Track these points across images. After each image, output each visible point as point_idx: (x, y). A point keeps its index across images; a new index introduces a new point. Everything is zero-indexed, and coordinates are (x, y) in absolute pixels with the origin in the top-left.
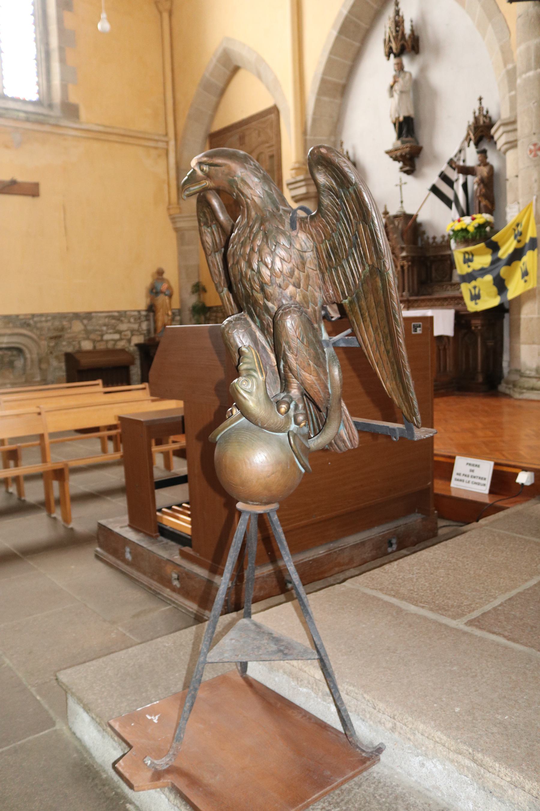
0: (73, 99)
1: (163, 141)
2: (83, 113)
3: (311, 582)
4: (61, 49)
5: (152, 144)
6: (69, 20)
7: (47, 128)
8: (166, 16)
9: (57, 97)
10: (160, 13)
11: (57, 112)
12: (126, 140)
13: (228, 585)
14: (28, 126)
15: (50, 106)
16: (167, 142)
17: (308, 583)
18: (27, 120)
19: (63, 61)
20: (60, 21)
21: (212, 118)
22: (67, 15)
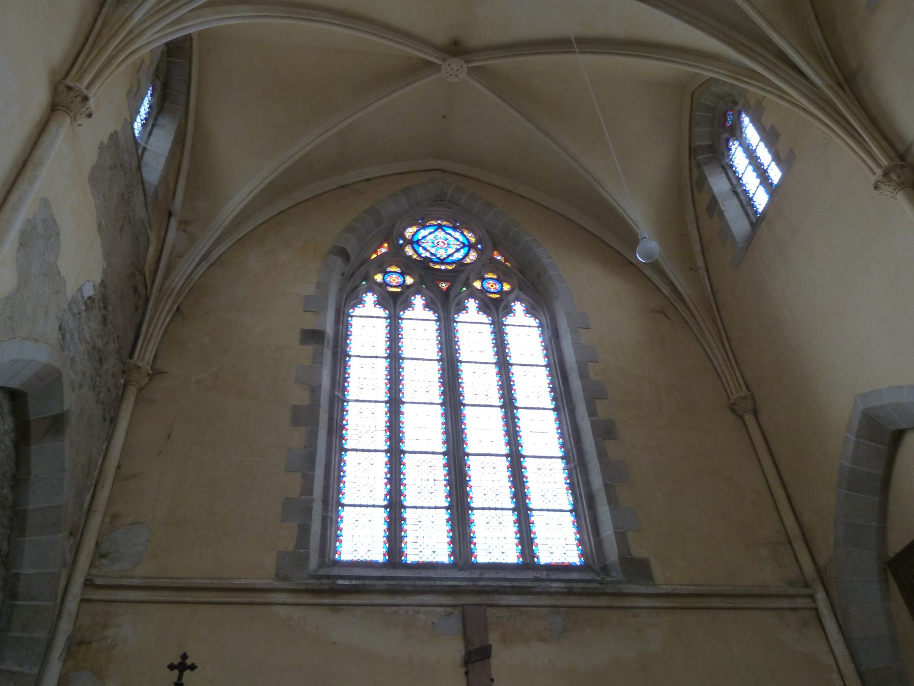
0: (638, 551)
1: (802, 596)
2: (657, 570)
3: (110, 496)
4: (608, 487)
5: (786, 603)
6: (612, 447)
7: (603, 601)
8: (749, 418)
9: (612, 553)
10: (741, 417)
11: (617, 575)
12: (739, 602)
13: (103, 267)
14: (573, 601)
15: (605, 569)
16: (812, 597)
17: (112, 489)
18: (570, 593)
19: (612, 501)
20: (602, 454)
21: (882, 532)
22: (611, 446)
